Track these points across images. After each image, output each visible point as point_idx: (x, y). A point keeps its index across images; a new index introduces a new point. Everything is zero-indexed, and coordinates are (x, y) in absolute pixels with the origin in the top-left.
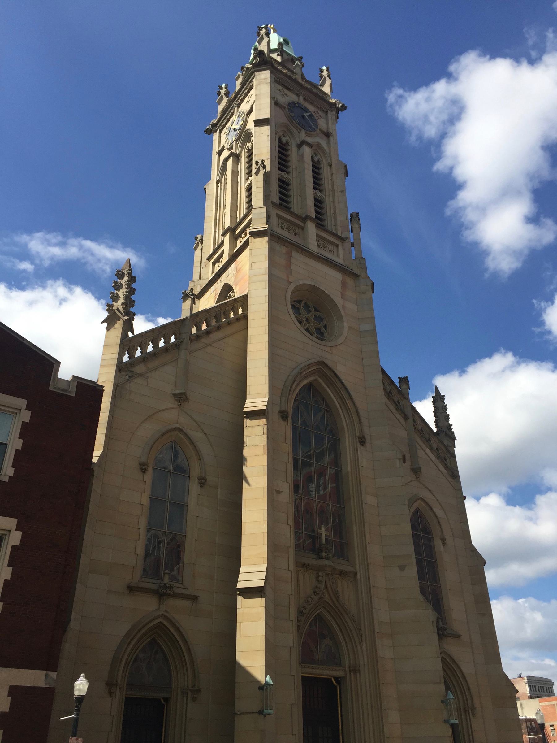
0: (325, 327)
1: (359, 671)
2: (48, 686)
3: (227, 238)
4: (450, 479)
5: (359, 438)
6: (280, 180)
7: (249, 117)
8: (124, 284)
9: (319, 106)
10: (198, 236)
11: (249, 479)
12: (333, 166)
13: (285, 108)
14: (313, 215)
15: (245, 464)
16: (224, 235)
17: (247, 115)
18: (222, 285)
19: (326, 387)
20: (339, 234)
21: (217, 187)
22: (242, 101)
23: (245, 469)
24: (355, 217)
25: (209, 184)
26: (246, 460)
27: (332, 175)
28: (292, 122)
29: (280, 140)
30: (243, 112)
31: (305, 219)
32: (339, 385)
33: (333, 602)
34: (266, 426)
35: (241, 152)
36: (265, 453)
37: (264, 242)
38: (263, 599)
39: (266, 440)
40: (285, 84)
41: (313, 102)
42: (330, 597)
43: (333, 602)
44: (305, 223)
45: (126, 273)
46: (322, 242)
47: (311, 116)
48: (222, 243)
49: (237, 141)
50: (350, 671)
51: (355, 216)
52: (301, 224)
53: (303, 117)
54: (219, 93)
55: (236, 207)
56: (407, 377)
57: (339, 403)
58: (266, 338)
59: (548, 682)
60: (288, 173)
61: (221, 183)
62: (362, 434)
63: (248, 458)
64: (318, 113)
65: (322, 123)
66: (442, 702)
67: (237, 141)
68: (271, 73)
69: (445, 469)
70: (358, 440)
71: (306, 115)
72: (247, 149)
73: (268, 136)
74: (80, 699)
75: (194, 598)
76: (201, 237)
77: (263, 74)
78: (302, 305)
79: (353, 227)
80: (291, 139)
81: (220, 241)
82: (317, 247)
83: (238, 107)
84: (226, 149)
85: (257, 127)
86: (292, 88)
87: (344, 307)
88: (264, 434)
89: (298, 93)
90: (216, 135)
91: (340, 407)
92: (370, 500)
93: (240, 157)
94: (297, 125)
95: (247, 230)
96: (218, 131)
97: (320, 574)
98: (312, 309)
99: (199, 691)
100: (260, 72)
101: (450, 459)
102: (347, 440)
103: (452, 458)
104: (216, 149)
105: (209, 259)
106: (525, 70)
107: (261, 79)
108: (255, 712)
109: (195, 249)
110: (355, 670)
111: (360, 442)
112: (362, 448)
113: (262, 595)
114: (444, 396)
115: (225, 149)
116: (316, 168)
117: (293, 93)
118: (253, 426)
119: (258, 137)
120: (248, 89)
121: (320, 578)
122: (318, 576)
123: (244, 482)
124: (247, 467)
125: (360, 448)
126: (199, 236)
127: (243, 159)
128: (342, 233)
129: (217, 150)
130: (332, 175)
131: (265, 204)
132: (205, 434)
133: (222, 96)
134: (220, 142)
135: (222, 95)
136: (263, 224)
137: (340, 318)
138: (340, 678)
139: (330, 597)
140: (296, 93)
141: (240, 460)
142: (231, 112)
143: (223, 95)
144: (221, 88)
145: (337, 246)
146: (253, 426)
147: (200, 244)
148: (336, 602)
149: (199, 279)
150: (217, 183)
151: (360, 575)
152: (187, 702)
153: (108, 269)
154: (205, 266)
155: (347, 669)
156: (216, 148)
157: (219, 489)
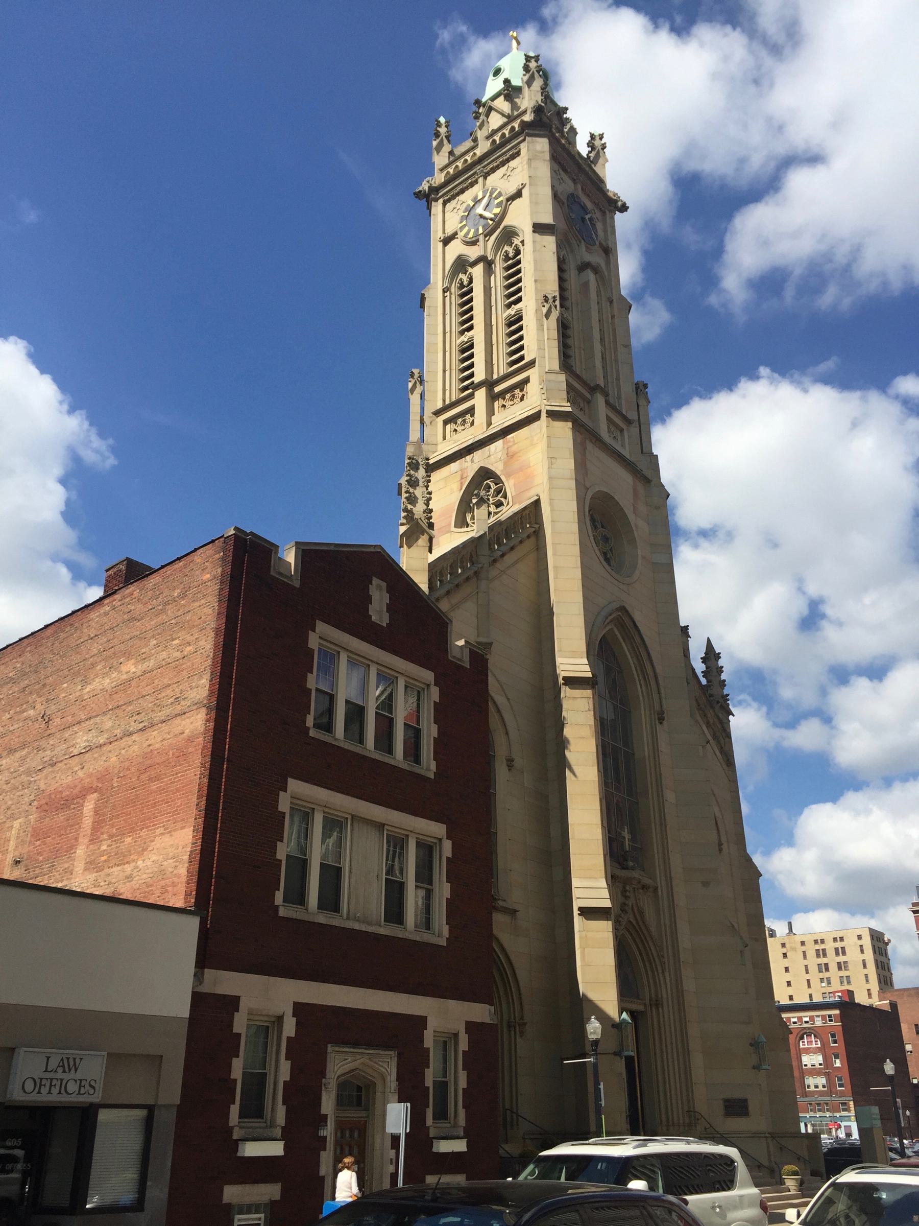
0: (611, 550)
1: (662, 1005)
2: (492, 1022)
4: (724, 766)
5: (658, 714)
7: (510, 205)
8: (420, 478)
9: (597, 202)
10: (414, 370)
11: (575, 768)
12: (615, 304)
13: (563, 204)
15: (567, 748)
17: (508, 200)
18: (476, 467)
19: (622, 640)
20: (624, 413)
21: (444, 297)
22: (493, 170)
23: (567, 753)
24: (640, 389)
25: (429, 288)
26: (568, 742)
27: (613, 317)
28: (572, 229)
30: (500, 194)
32: (638, 640)
33: (638, 923)
34: (592, 699)
35: (495, 258)
36: (592, 736)
37: (567, 430)
39: (592, 718)
40: (562, 162)
41: (590, 195)
42: (635, 916)
43: (638, 923)
44: (592, 395)
45: (421, 463)
47: (591, 219)
49: (485, 236)
50: (651, 1005)
51: (642, 387)
52: (588, 396)
53: (583, 219)
54: (437, 135)
55: (490, 348)
56: (688, 626)
57: (634, 663)
58: (578, 573)
61: (451, 294)
63: (570, 739)
64: (595, 213)
66: (751, 1045)
67: (485, 236)
69: (721, 753)
70: (656, 717)
71: (587, 217)
72: (503, 255)
73: (554, 253)
74: (596, 1043)
75: (514, 912)
76: (419, 373)
77: (538, 142)
79: (640, 403)
80: (569, 255)
83: (485, 178)
84: (459, 239)
85: (537, 235)
86: (569, 170)
87: (636, 526)
88: (589, 710)
89: (575, 178)
90: (437, 206)
91: (636, 668)
92: (670, 796)
93: (493, 265)
94: (577, 234)
95: (516, 391)
96: (441, 201)
97: (628, 888)
98: (599, 526)
99: (525, 1024)
100: (534, 139)
101: (724, 739)
102: (643, 713)
103: (727, 739)
105: (438, 413)
106: (664, 40)
107: (536, 151)
108: (609, 1053)
109: (412, 390)
110: (657, 1003)
111: (659, 719)
112: (660, 726)
113: (607, 918)
114: (720, 653)
115: (457, 238)
117: (569, 177)
118: (575, 698)
119: (539, 251)
120: (508, 156)
121: (628, 894)
122: (624, 888)
123: (567, 772)
124: (570, 751)
125: (659, 726)
126: (416, 371)
128: (626, 412)
129: (440, 234)
130: (613, 317)
132: (508, 699)
133: (442, 140)
135: (442, 138)
136: (562, 399)
137: (633, 541)
138: (637, 1012)
139: (635, 916)
140: (573, 178)
141: (562, 744)
142: (470, 181)
143: (444, 138)
144: (439, 125)
145: (622, 431)
146: (575, 698)
148: (641, 923)
150: (444, 291)
151: (662, 891)
152: (515, 1038)
154: (431, 423)
155: (648, 1002)
156: (437, 233)
157: (525, 774)
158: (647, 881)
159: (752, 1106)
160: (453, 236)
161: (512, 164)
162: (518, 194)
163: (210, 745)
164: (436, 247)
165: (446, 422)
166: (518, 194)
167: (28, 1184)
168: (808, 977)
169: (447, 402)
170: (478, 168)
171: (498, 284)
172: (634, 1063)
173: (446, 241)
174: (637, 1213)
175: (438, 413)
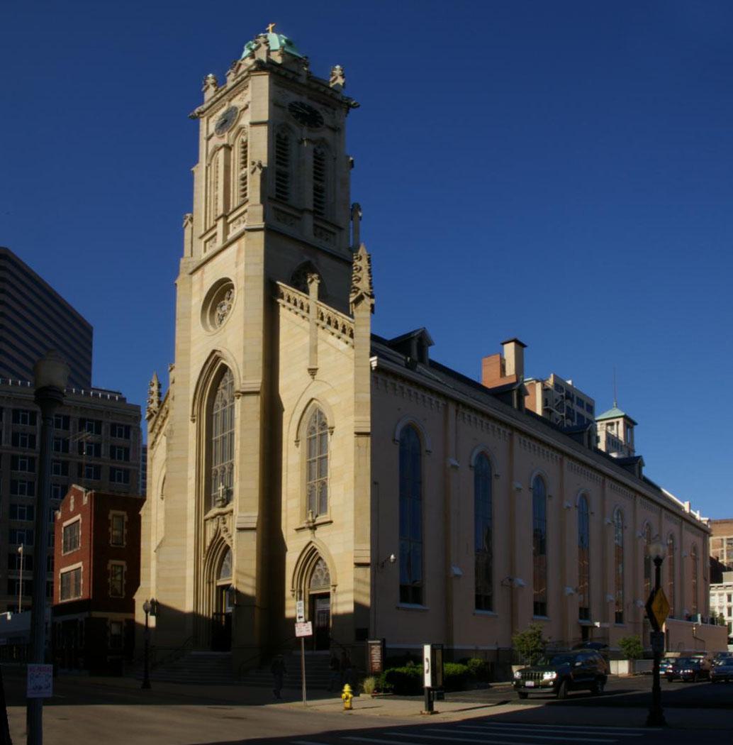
3: (220, 223)
6: (278, 173)
14: (312, 208)
16: (217, 220)
22: (234, 96)
29: (278, 136)
31: (302, 211)
38: (369, 558)
46: (319, 230)
48: (215, 226)
59: (25, 394)
60: (286, 166)
62: (312, 382)
65: (327, 119)
68: (270, 78)
78: (224, 464)
81: (212, 225)
82: (313, 236)
83: (230, 100)
104: (203, 134)
105: (201, 237)
116: (319, 161)
127: (236, 153)
131: (262, 202)
134: (208, 129)
147: (189, 223)
149: (190, 255)
150: (207, 168)
153: (446, 698)
158: (305, 302)
159: (236, 530)
160: (212, 135)
161: (245, 92)
162: (246, 107)
163: (408, 697)
164: (203, 142)
165: (206, 242)
166: (246, 107)
167: (565, 664)
168: (731, 604)
169: (208, 228)
170: (225, 98)
171: (236, 156)
172: (678, 498)
173: (208, 139)
174: (404, 358)
175: (201, 237)
